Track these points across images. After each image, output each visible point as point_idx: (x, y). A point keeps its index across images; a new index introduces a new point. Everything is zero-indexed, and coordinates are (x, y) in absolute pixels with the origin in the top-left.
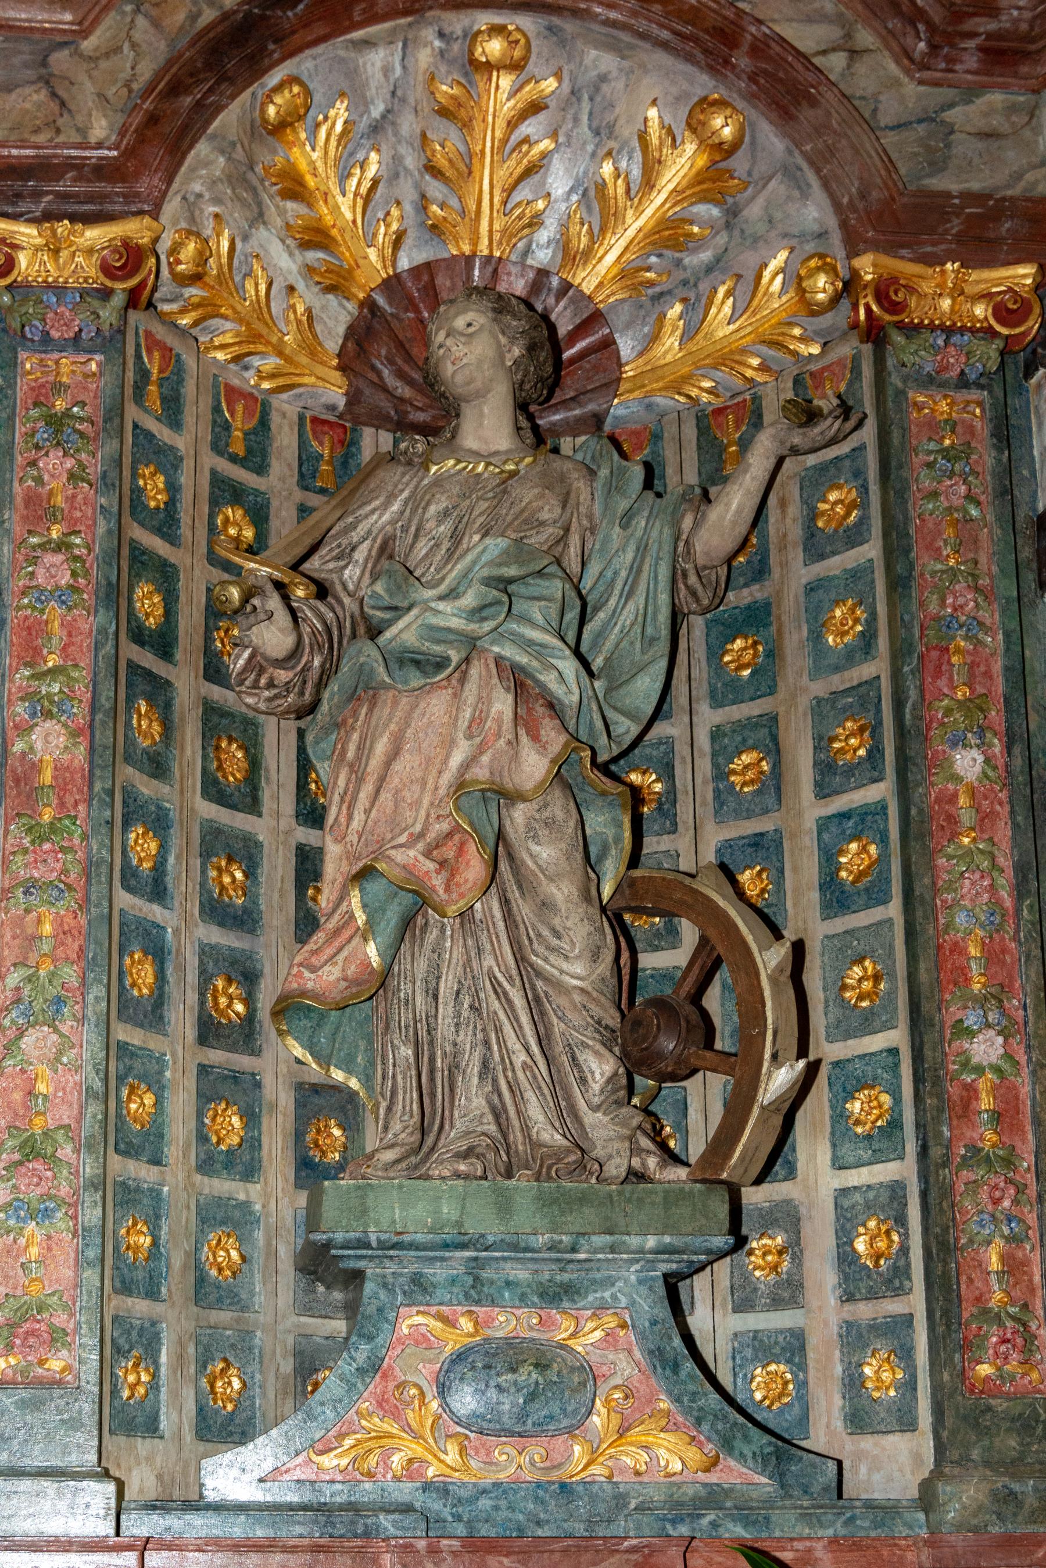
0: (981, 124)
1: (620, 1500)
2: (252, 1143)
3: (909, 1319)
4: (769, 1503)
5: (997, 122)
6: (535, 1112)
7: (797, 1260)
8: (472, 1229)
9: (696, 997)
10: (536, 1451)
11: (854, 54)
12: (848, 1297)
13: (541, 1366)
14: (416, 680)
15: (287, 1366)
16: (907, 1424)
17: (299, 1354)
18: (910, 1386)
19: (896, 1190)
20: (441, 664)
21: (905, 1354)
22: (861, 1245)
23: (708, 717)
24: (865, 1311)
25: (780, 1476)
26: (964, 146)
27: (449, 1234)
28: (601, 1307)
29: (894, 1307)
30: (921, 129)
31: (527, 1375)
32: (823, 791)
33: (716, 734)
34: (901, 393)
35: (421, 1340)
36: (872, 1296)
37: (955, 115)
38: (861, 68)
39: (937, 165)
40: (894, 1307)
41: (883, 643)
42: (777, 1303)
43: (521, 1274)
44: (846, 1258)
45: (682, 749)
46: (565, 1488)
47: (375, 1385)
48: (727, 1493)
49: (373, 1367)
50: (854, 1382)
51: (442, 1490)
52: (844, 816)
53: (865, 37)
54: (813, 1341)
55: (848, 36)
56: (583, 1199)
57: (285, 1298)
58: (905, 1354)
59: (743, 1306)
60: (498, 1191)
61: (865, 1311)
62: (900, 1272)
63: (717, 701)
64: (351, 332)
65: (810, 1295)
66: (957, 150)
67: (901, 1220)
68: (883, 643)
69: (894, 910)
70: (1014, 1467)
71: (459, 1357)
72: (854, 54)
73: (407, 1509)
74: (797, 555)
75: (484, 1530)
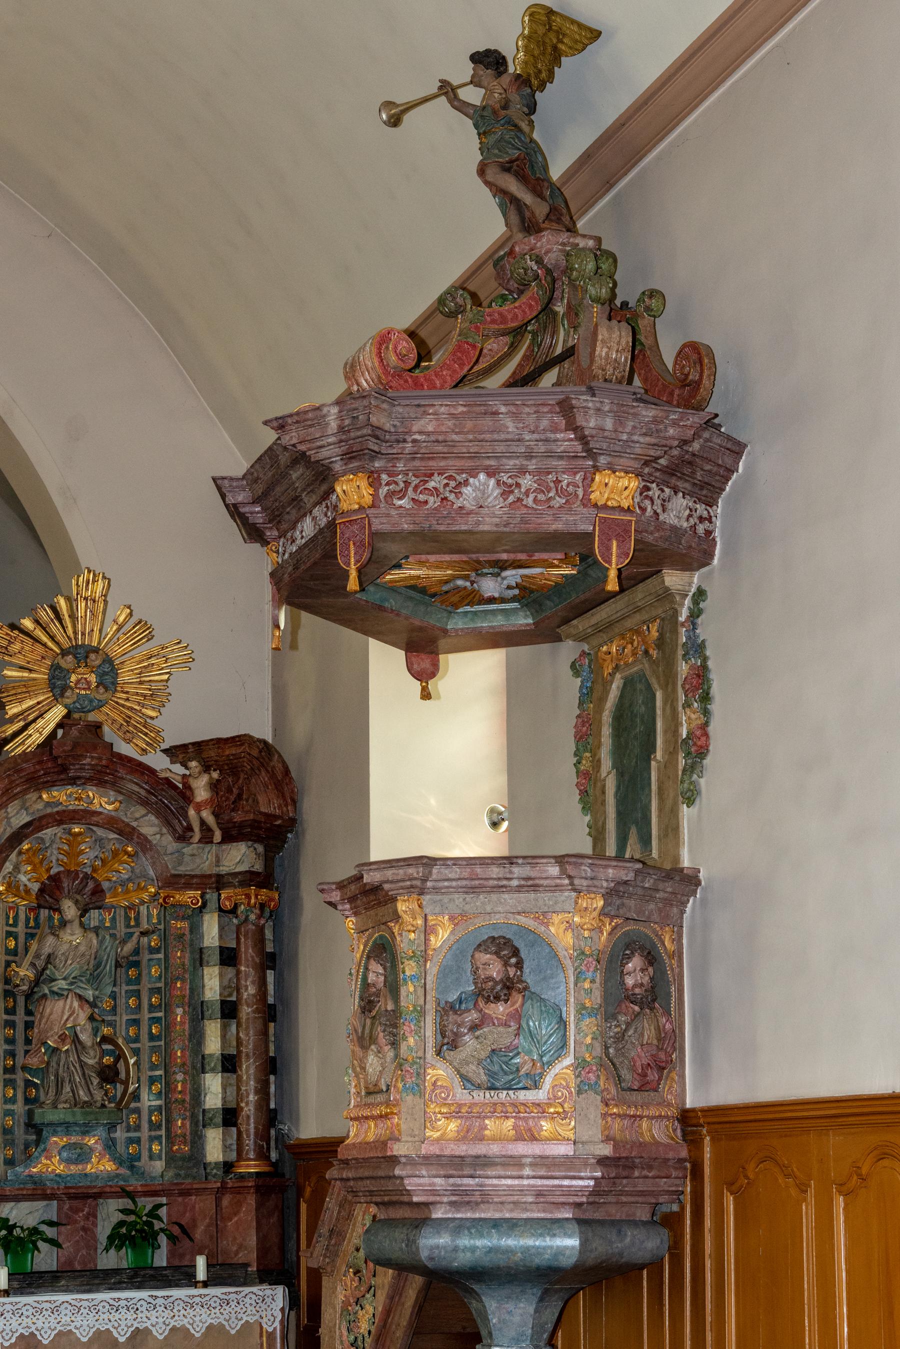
0: (191, 852)
1: (97, 1177)
2: (15, 1095)
3: (161, 1136)
4: (129, 1177)
5: (195, 852)
6: (81, 1093)
7: (140, 1121)
8: (67, 1120)
9: (116, 1066)
10: (80, 1167)
11: (162, 835)
12: (150, 1130)
13: (81, 1149)
14: (56, 998)
15: (22, 1147)
16: (161, 1159)
17: (25, 1144)
18: (161, 1150)
19: (160, 1106)
20: (62, 995)
21: (161, 1144)
22: (153, 1118)
23: (125, 988)
24: (153, 1133)
25: (132, 1171)
26: (187, 859)
27: (62, 1121)
28: (94, 1136)
29: (159, 1133)
30: (177, 855)
31: (78, 1151)
32: (150, 1012)
33: (126, 992)
34: (169, 922)
35: (56, 1142)
36: (155, 1130)
37: (185, 850)
38: (163, 838)
39: (180, 863)
40: (159, 1133)
41: (163, 979)
42: (135, 1131)
43: (78, 1129)
44: (150, 1121)
45: (118, 995)
46: (86, 1175)
47: (45, 1153)
48: (120, 1175)
49: (45, 1150)
50: (150, 1149)
51: (59, 1175)
52: (154, 1018)
53: (164, 830)
54: (142, 1139)
55: (161, 830)
56: (91, 1113)
57: (22, 1131)
58: (161, 1144)
59: (128, 1131)
60: (73, 1112)
61: (153, 1133)
62: (160, 1125)
63: (127, 985)
64: (39, 890)
65: (142, 1130)
66: (185, 860)
67: (161, 1114)
68: (163, 979)
69: (162, 1043)
70: (181, 1168)
71: (64, 1147)
72: (162, 835)
73: (52, 1180)
74: (147, 952)
75: (69, 1185)
